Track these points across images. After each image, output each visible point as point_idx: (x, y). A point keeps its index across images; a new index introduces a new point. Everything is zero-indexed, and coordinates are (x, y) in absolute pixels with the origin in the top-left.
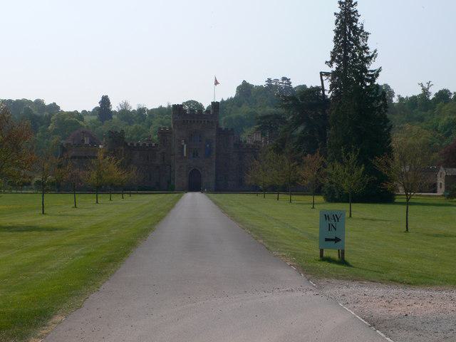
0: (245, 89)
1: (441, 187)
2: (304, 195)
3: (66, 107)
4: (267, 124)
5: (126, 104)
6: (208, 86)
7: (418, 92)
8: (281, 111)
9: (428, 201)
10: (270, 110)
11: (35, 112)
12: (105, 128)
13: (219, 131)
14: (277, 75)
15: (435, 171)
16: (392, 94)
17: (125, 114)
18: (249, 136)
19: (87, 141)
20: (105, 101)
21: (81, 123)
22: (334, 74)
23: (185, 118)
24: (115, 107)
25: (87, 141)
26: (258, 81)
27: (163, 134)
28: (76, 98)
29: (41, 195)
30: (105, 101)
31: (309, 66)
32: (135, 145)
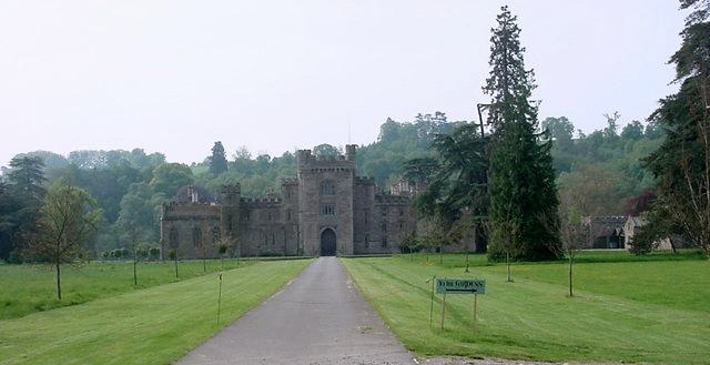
0: (391, 130)
1: (473, 287)
2: (678, 260)
3: (171, 159)
4: (417, 169)
5: (244, 151)
6: (352, 125)
7: (603, 125)
8: (434, 153)
9: (595, 256)
10: (419, 153)
11: (135, 166)
12: (219, 181)
13: (358, 181)
14: (429, 109)
15: (623, 223)
16: (570, 128)
17: (243, 164)
18: (397, 187)
19: (195, 198)
20: (218, 148)
21: (189, 176)
22: (492, 107)
23: (320, 166)
24: (230, 157)
25: (195, 198)
26: (406, 117)
27: (289, 186)
28: (188, 152)
29: (55, 266)
30: (218, 148)
31: (463, 99)
32: (254, 200)
